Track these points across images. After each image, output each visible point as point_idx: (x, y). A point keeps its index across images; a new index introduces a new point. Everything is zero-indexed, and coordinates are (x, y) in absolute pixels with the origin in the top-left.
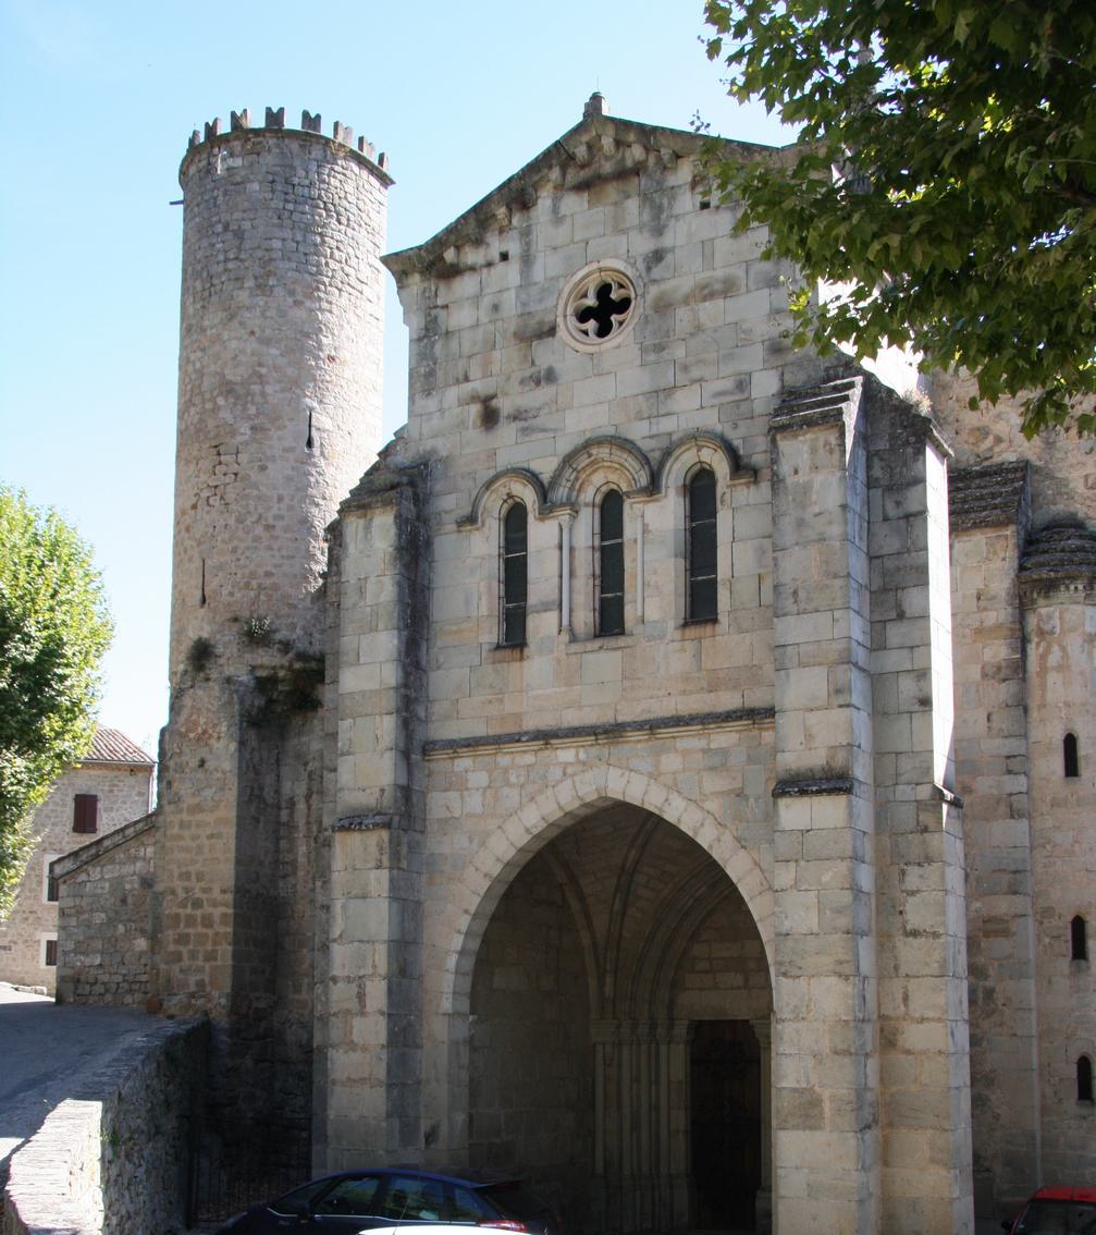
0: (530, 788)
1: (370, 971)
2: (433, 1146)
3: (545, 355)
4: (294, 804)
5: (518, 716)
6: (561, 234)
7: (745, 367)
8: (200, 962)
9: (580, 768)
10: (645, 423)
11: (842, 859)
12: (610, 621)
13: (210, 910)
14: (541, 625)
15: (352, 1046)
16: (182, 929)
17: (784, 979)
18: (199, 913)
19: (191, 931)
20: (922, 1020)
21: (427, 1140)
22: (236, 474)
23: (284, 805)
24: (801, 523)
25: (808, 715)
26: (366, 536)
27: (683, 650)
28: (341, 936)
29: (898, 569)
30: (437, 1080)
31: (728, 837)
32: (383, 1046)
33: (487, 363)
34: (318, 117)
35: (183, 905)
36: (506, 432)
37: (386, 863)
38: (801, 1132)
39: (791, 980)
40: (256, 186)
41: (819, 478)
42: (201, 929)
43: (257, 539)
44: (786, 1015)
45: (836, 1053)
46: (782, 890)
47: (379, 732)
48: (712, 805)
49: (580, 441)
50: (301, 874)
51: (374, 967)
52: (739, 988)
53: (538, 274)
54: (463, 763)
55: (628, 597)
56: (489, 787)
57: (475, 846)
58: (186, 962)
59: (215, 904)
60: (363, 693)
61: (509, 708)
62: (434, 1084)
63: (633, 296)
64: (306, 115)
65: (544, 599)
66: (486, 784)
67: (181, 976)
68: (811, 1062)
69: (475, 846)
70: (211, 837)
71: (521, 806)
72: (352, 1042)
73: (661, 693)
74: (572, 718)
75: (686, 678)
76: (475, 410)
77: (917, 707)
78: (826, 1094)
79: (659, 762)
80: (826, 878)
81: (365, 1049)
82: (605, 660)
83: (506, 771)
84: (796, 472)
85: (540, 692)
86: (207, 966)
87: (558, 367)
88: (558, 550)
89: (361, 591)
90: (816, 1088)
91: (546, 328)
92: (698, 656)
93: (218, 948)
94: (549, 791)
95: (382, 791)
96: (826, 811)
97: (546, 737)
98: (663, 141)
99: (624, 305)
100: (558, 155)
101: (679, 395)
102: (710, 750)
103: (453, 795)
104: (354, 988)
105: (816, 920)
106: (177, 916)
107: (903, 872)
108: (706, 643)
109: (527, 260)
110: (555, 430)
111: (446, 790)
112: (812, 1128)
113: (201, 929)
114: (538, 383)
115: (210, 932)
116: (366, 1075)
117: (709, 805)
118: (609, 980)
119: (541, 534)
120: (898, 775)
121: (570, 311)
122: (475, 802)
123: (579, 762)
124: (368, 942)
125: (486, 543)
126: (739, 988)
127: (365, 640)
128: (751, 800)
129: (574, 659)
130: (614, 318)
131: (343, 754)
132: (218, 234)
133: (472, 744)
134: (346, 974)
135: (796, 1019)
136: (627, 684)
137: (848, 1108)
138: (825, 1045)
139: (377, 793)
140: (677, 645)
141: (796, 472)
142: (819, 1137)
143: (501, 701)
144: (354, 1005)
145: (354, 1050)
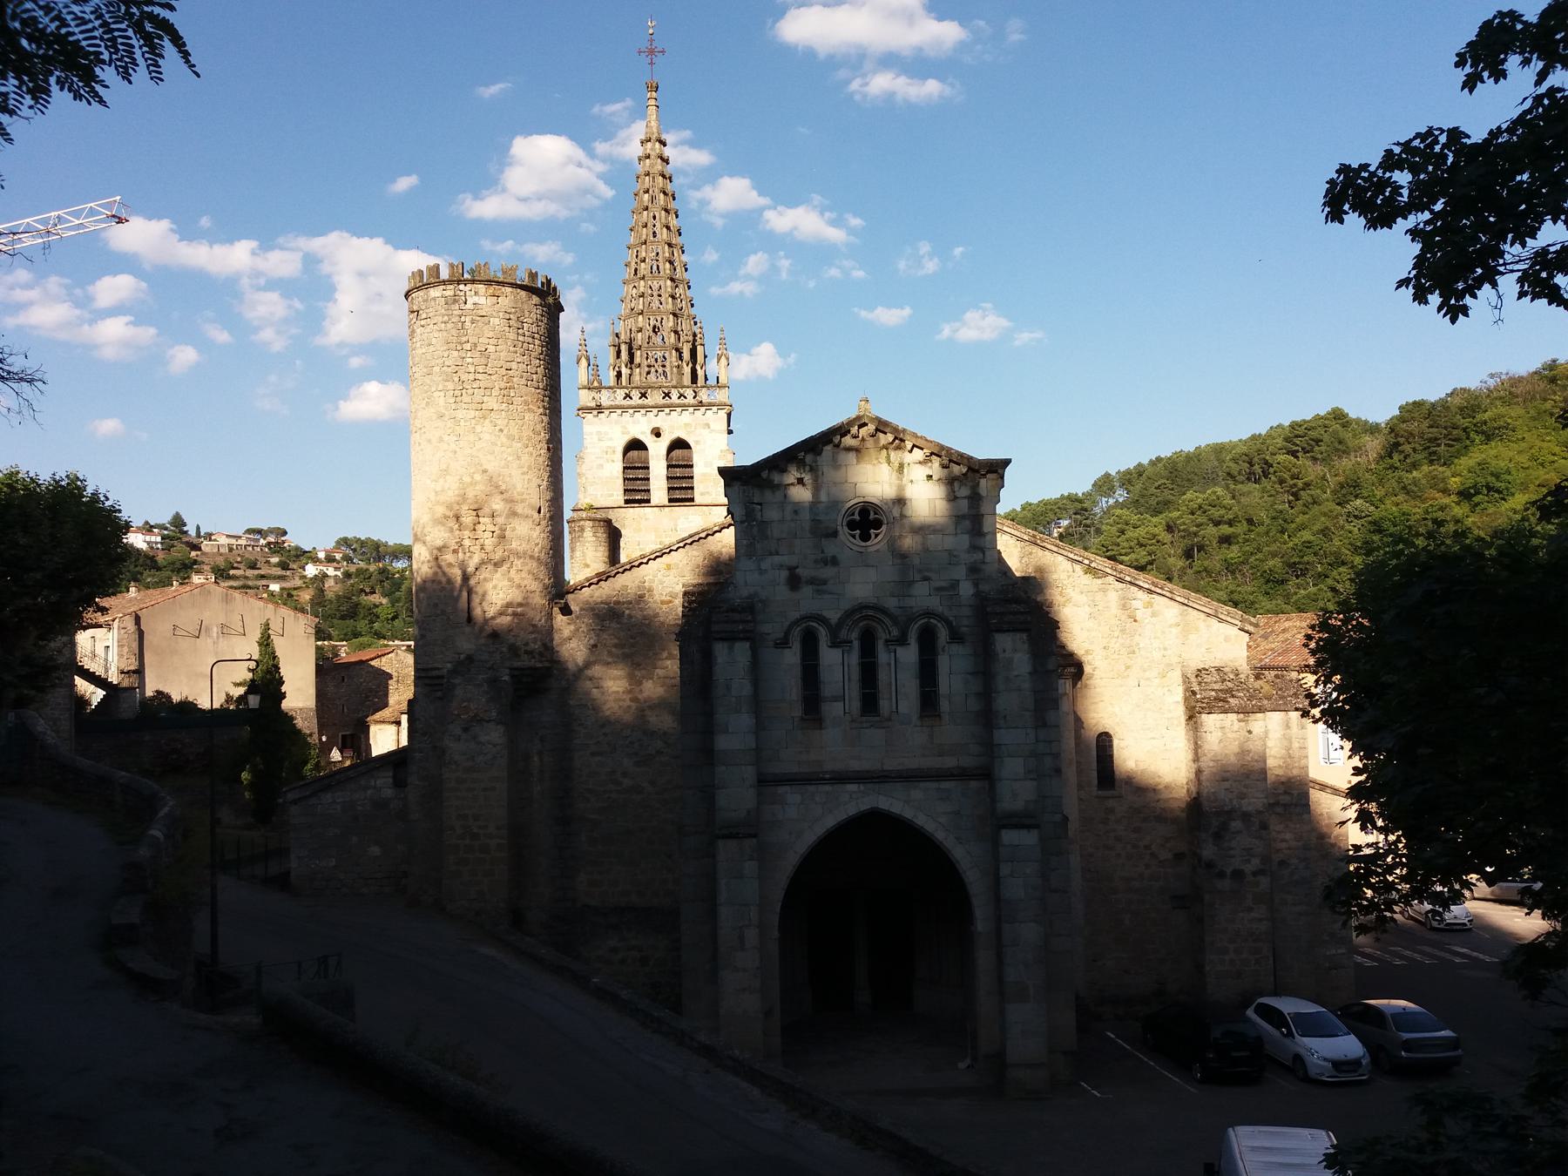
3: (831, 548)
12: (870, 703)
14: (832, 710)
34: (1336, 215)
36: (807, 591)
54: (781, 790)
74: (855, 765)
76: (785, 574)
88: (836, 664)
96: (1028, 838)
97: (841, 778)
98: (907, 437)
101: (917, 585)
119: (830, 657)
125: (792, 657)
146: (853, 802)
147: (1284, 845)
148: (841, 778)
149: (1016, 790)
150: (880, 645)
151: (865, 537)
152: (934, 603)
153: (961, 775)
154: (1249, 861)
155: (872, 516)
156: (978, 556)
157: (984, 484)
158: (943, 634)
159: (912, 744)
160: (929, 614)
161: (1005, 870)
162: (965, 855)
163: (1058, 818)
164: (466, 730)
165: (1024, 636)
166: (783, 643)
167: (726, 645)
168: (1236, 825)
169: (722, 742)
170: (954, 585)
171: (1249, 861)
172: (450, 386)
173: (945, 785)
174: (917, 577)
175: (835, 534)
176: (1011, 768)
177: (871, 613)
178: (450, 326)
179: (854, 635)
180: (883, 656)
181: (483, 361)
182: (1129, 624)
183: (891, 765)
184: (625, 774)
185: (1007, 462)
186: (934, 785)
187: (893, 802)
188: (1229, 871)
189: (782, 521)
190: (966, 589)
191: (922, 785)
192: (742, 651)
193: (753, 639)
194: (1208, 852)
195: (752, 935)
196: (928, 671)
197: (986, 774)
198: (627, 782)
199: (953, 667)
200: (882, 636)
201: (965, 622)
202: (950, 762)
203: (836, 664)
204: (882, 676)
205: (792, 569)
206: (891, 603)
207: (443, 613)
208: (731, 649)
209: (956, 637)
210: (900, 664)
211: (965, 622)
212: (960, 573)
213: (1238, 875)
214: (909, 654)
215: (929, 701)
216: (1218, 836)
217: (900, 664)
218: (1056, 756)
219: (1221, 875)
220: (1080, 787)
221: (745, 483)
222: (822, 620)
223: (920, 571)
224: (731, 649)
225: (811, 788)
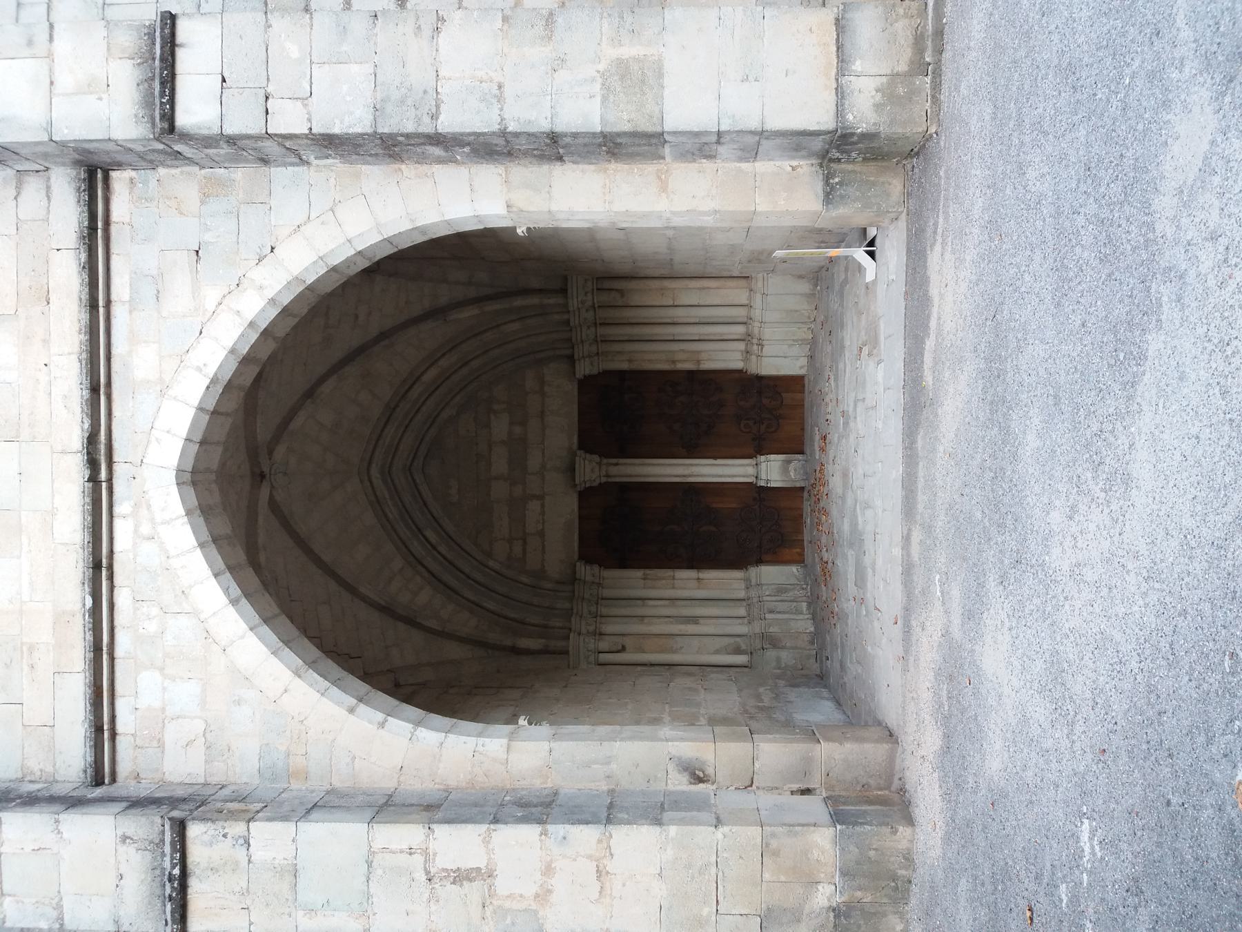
1: (418, 859)
2: (710, 771)
17: (442, 118)
21: (701, 780)
25: (58, 88)
31: (258, 274)
32: (544, 833)
37: (238, 828)
38: (666, 92)
39: (443, 107)
45: (550, 38)
46: (309, 120)
47: (29, 847)
48: (211, 296)
52: (543, 506)
56: (162, 669)
62: (614, 766)
66: (157, 674)
68: (562, 75)
71: (194, 613)
78: (611, 53)
80: (294, 51)
81: (548, 870)
90: (601, 67)
95: (125, 838)
97: (99, 566)
102: (132, 300)
103: (172, 735)
105: (355, 68)
111: (161, 745)
112: (660, 75)
116: (592, 867)
117: (210, 305)
118: (524, 643)
124: (370, 864)
126: (543, 506)
128: (208, 237)
131: (60, 919)
133: (100, 696)
135: (500, 99)
137: (629, 18)
143: (31, 649)
144: (473, 891)
148: (99, 566)
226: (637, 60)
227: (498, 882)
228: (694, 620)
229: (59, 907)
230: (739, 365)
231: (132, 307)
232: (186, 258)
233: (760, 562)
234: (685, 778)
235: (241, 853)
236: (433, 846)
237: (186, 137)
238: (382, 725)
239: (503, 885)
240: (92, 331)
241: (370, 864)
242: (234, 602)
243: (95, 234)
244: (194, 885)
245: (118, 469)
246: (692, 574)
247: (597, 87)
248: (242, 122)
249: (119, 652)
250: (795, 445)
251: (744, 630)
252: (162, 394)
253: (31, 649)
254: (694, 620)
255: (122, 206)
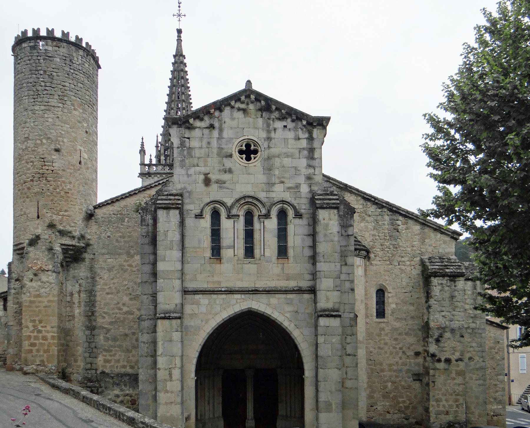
0: (224, 306)
1: (174, 366)
4: (73, 295)
5: (219, 282)
6: (234, 123)
7: (298, 182)
8: (41, 353)
9: (242, 300)
10: (265, 193)
11: (339, 335)
12: (249, 252)
13: (46, 334)
14: (227, 253)
15: (167, 392)
16: (32, 340)
18: (40, 335)
19: (37, 342)
20: (351, 379)
21: (186, 419)
22: (52, 171)
23: (68, 295)
24: (325, 235)
25: (328, 293)
26: (167, 216)
27: (278, 267)
28: (161, 354)
29: (345, 250)
30: (190, 400)
31: (292, 325)
33: (206, 161)
35: (32, 332)
40: (58, 60)
41: (331, 222)
42: (41, 341)
43: (62, 197)
44: (321, 380)
48: (288, 315)
49: (242, 195)
50: (76, 320)
51: (175, 364)
53: (225, 135)
55: (255, 247)
57: (204, 323)
58: (35, 353)
59: (48, 332)
60: (167, 271)
61: (216, 279)
63: (260, 150)
64: (63, 32)
65: (229, 245)
67: (32, 358)
68: (329, 393)
69: (204, 323)
70: (46, 307)
71: (221, 311)
72: (167, 390)
73: (270, 279)
75: (279, 275)
76: (202, 177)
77: (350, 291)
78: (333, 403)
79: (270, 301)
80: (334, 340)
81: (172, 392)
82: (250, 267)
83: (215, 299)
84: (324, 219)
85: (228, 275)
86: (45, 355)
87: (233, 168)
88: (232, 230)
89: (166, 236)
91: (228, 154)
92: (283, 269)
93: (51, 348)
94: (231, 307)
95: (176, 305)
96: (335, 322)
97: (230, 292)
99: (256, 152)
100: (236, 97)
101: (276, 185)
104: (167, 372)
106: (30, 336)
107: (346, 338)
108: (286, 265)
109: (221, 130)
110: (232, 189)
112: (329, 412)
113: (41, 341)
114: (225, 172)
115: (46, 342)
119: (226, 224)
120: (345, 310)
121: (237, 150)
122: (203, 309)
123: (242, 298)
124: (173, 356)
127: (168, 252)
128: (300, 314)
129: (240, 265)
130: (252, 156)
132: (41, 75)
134: (164, 367)
135: (325, 381)
136: (258, 275)
138: (333, 389)
139: (174, 306)
140: (276, 265)
141: (324, 219)
142: (331, 415)
143: (213, 276)
144: (168, 377)
145: (168, 393)
146: (238, 305)
147: (471, 349)
148: (230, 292)
149: (327, 299)
150: (256, 219)
151: (248, 159)
152: (287, 196)
153: (300, 291)
154: (453, 354)
155: (252, 148)
156: (311, 171)
157: (316, 133)
158: (291, 213)
159: (269, 271)
160: (283, 202)
161: (321, 340)
162: (300, 336)
163: (352, 315)
164: (35, 275)
165: (336, 211)
166: (200, 216)
167: (165, 211)
168: (447, 335)
169: (161, 266)
170: (298, 186)
171: (453, 354)
172: (32, 93)
173: (290, 296)
174: (277, 181)
175: (231, 156)
176: (325, 284)
177: (250, 200)
178: (32, 61)
179: (242, 213)
180: (257, 225)
181: (50, 80)
182: (396, 234)
183: (260, 285)
184: (124, 304)
185: (328, 119)
186: (284, 296)
187: (260, 305)
188: (443, 359)
189: (201, 148)
190: (305, 189)
191: (277, 296)
192: (174, 214)
193: (180, 208)
194: (433, 348)
195: (176, 374)
196: (282, 234)
197: (313, 291)
198: (125, 309)
199: (297, 230)
200: (256, 213)
201: (304, 207)
202: (292, 284)
203: (232, 230)
204: (257, 236)
205: (206, 175)
206: (262, 196)
207: (25, 214)
208: (168, 214)
209: (298, 215)
210: (267, 230)
211: (304, 207)
212: (301, 179)
213: (448, 361)
214: (272, 224)
215: (282, 251)
216: (438, 341)
217: (267, 230)
218: (352, 282)
219: (439, 361)
220: (367, 316)
221: (180, 126)
222: (222, 204)
223: (279, 178)
224: (168, 214)
225: (214, 296)
226: (332, 407)
227: (169, 382)
228: (209, 404)
229: (162, 291)
230: (279, 414)
231: (285, 298)
232: (296, 309)
233: (224, 420)
234: (186, 416)
235: (174, 330)
236: (177, 369)
237: (317, 319)
238: (197, 351)
239: (169, 384)
240: (280, 291)
241: (173, 356)
242: (223, 320)
243: (300, 291)
244: (168, 320)
245: (251, 296)
246: (221, 402)
247: (327, 400)
248: (320, 330)
249: (212, 295)
250: (245, 247)
251: (207, 417)
252: (267, 304)
253: (213, 276)
254: (209, 404)
255: (306, 296)
